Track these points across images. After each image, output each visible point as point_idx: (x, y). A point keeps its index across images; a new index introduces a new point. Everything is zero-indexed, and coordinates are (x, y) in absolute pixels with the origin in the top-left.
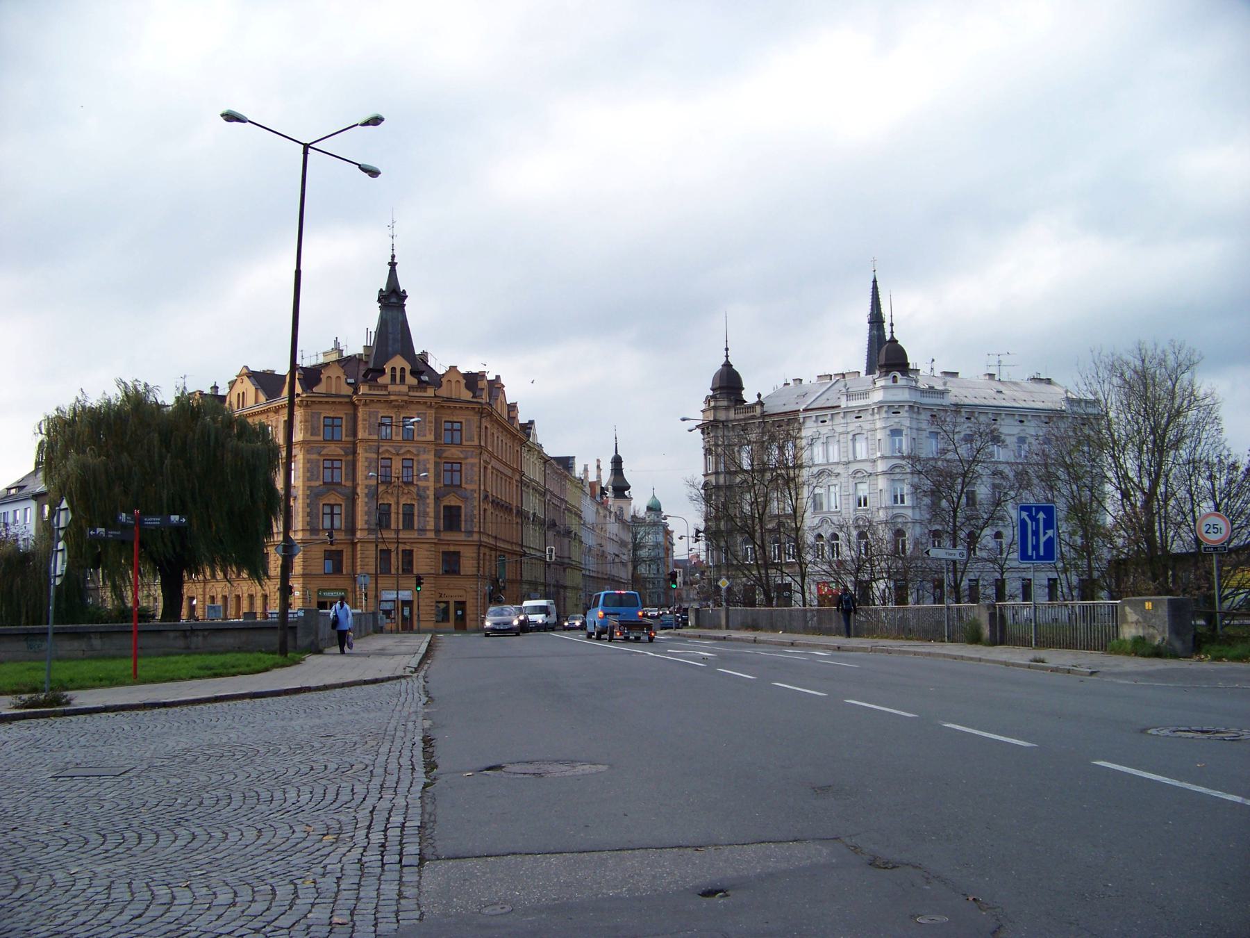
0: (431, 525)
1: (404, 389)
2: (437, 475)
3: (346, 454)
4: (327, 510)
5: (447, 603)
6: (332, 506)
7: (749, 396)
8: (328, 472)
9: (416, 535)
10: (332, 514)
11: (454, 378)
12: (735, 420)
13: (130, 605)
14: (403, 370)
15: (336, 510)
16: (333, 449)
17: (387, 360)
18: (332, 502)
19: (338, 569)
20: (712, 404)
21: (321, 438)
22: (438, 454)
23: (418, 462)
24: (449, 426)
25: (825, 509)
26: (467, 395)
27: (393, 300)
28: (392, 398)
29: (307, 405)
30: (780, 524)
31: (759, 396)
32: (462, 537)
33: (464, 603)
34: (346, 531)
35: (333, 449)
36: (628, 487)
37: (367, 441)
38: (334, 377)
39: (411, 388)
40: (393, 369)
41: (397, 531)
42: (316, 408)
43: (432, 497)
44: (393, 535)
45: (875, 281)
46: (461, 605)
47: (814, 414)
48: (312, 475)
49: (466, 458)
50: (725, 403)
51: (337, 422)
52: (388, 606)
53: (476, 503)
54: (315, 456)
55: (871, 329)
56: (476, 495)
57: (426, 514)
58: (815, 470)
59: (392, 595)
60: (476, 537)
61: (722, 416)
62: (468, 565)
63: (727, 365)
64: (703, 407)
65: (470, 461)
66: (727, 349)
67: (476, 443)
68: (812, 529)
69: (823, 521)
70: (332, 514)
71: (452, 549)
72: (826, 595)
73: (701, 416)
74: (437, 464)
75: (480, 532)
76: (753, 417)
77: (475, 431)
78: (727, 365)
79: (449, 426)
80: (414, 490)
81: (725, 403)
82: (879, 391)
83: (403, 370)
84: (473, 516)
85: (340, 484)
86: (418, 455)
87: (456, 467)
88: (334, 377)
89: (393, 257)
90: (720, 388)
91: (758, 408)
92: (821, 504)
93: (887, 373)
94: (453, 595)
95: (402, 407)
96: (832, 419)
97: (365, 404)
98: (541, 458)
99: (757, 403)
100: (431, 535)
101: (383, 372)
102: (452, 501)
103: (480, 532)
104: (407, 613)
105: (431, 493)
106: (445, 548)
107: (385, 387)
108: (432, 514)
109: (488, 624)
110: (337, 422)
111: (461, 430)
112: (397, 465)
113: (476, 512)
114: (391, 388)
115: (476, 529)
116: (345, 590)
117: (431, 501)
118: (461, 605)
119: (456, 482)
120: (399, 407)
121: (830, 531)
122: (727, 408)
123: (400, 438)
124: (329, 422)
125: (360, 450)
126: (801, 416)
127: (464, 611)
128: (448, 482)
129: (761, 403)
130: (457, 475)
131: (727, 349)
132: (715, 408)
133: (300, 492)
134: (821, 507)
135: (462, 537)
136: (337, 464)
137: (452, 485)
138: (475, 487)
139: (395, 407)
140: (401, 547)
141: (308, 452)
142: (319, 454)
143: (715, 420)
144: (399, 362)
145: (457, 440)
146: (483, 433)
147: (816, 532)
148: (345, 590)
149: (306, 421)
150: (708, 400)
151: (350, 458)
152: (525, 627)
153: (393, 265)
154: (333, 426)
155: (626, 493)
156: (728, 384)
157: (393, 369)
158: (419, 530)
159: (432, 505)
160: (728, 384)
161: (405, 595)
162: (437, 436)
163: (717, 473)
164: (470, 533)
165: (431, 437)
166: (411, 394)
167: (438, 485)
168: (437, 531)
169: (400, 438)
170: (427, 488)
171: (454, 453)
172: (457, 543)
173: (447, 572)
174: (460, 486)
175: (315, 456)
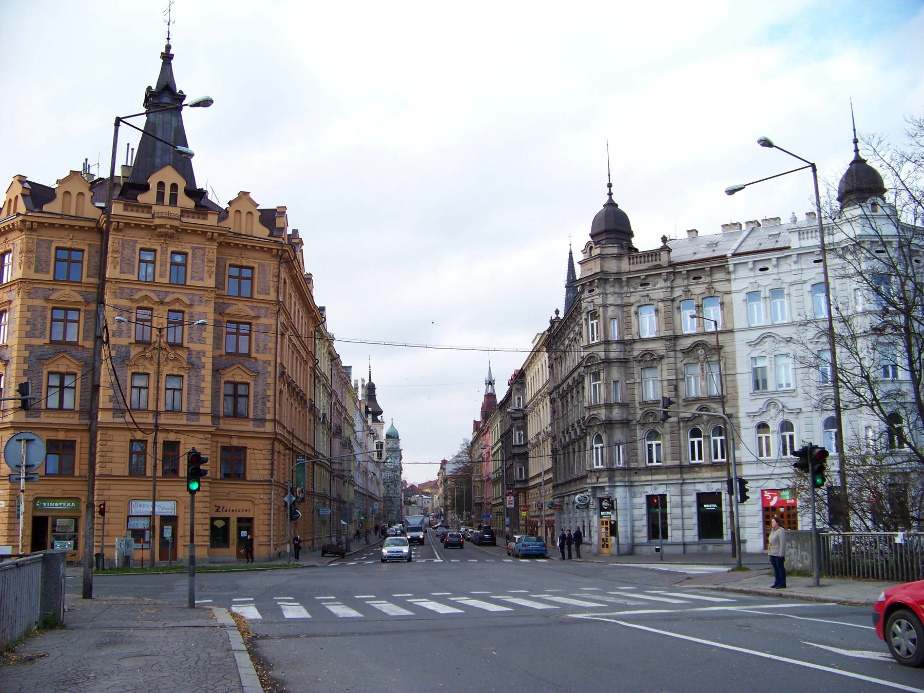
0: (207, 407)
1: (176, 211)
2: (217, 339)
3: (87, 302)
4: (55, 381)
5: (227, 520)
6: (62, 376)
8: (59, 327)
9: (184, 421)
10: (62, 387)
11: (244, 208)
13: (385, 551)
14: (174, 186)
15: (68, 381)
16: (67, 293)
17: (154, 170)
18: (62, 369)
19: (65, 471)
20: (597, 251)
21: (50, 277)
22: (220, 310)
23: (191, 314)
24: (235, 272)
25: (771, 386)
26: (262, 232)
27: (166, 99)
28: (157, 222)
29: (31, 229)
31: (664, 239)
32: (249, 427)
33: (250, 520)
34: (81, 412)
35: (67, 293)
36: (381, 412)
37: (118, 281)
38: (74, 193)
39: (184, 212)
40: (161, 184)
41: (157, 413)
42: (45, 234)
43: (209, 366)
44: (150, 419)
45: (571, 253)
46: (246, 523)
47: (750, 259)
48: (34, 328)
49: (258, 317)
50: (615, 251)
51: (75, 256)
52: (141, 524)
53: (270, 380)
54: (39, 302)
55: (567, 292)
56: (271, 369)
57: (200, 390)
58: (755, 335)
59: (145, 508)
60: (269, 427)
61: (612, 266)
62: (257, 463)
63: (611, 205)
65: (264, 321)
66: (610, 186)
67: (272, 297)
69: (770, 403)
70: (62, 387)
71: (235, 442)
72: (774, 509)
74: (217, 324)
75: (274, 421)
76: (659, 267)
77: (271, 281)
78: (611, 205)
79: (235, 272)
80: (183, 354)
81: (615, 251)
83: (174, 186)
84: (265, 398)
85: (75, 344)
86: (191, 306)
87: (244, 328)
88: (74, 193)
89: (168, 47)
90: (606, 231)
91: (664, 255)
93: (864, 200)
94: (235, 510)
95: (171, 237)
97: (117, 229)
98: (330, 353)
99: (662, 249)
100: (206, 421)
101: (146, 188)
102: (239, 376)
103: (274, 421)
104: (168, 533)
105: (208, 361)
106: (226, 441)
107: (149, 207)
108: (208, 391)
109: (385, 551)
110: (75, 256)
111: (252, 279)
112: (160, 318)
113: (270, 392)
114: (156, 209)
115: (269, 416)
116: (77, 500)
117: (207, 372)
118: (246, 523)
119: (243, 349)
120: (166, 236)
121: (780, 418)
122: (618, 257)
123: (166, 280)
124: (64, 255)
125: (108, 297)
126: (732, 261)
127: (250, 530)
128: (232, 350)
129: (666, 249)
130: (244, 340)
131: (610, 186)
132: (602, 257)
133: (15, 354)
134: (765, 387)
135: (249, 427)
136: (72, 316)
137: (236, 354)
138: (269, 357)
139: (161, 235)
140: (162, 437)
141: (29, 295)
142: (47, 299)
144: (169, 175)
145: (246, 292)
146: (282, 285)
147: (758, 420)
148: (77, 500)
149: (29, 251)
151: (93, 307)
153: (167, 57)
154: (70, 261)
155: (379, 417)
156: (613, 227)
157: (161, 184)
158: (189, 413)
159: (209, 378)
160: (613, 227)
161: (166, 508)
162: (220, 285)
164: (262, 421)
165: (211, 282)
166: (184, 219)
167: (218, 353)
168: (215, 417)
169: (166, 280)
170: (202, 353)
171: (241, 308)
172: (243, 435)
173: (227, 476)
174: (249, 355)
175: (39, 302)
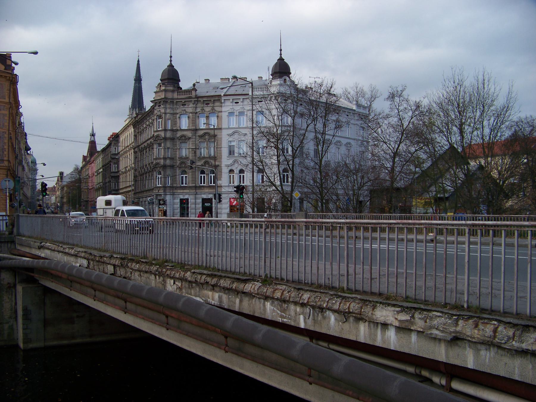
7: (185, 84)
12: (177, 99)
20: (163, 88)
30: (206, 163)
45: (138, 61)
47: (231, 98)
50: (171, 88)
53: (6, 141)
55: (135, 83)
56: (6, 136)
61: (169, 95)
63: (171, 66)
64: (155, 90)
67: (7, 100)
68: (228, 166)
73: (154, 95)
76: (190, 98)
81: (171, 88)
82: (276, 86)
90: (168, 79)
91: (193, 92)
92: (234, 151)
96: (243, 102)
99: (193, 89)
115: (6, 158)
122: (173, 91)
126: (223, 98)
132: (165, 91)
134: (234, 154)
143: (165, 98)
147: (230, 168)
150: (159, 86)
152: (412, 305)
163: (165, 130)
